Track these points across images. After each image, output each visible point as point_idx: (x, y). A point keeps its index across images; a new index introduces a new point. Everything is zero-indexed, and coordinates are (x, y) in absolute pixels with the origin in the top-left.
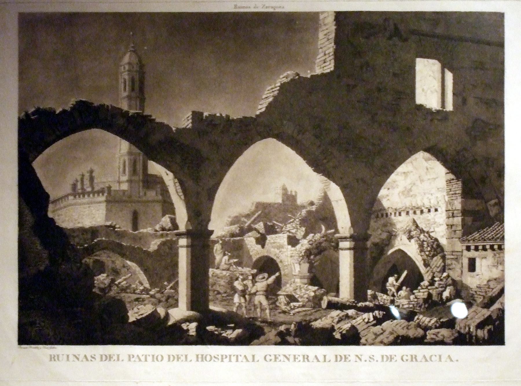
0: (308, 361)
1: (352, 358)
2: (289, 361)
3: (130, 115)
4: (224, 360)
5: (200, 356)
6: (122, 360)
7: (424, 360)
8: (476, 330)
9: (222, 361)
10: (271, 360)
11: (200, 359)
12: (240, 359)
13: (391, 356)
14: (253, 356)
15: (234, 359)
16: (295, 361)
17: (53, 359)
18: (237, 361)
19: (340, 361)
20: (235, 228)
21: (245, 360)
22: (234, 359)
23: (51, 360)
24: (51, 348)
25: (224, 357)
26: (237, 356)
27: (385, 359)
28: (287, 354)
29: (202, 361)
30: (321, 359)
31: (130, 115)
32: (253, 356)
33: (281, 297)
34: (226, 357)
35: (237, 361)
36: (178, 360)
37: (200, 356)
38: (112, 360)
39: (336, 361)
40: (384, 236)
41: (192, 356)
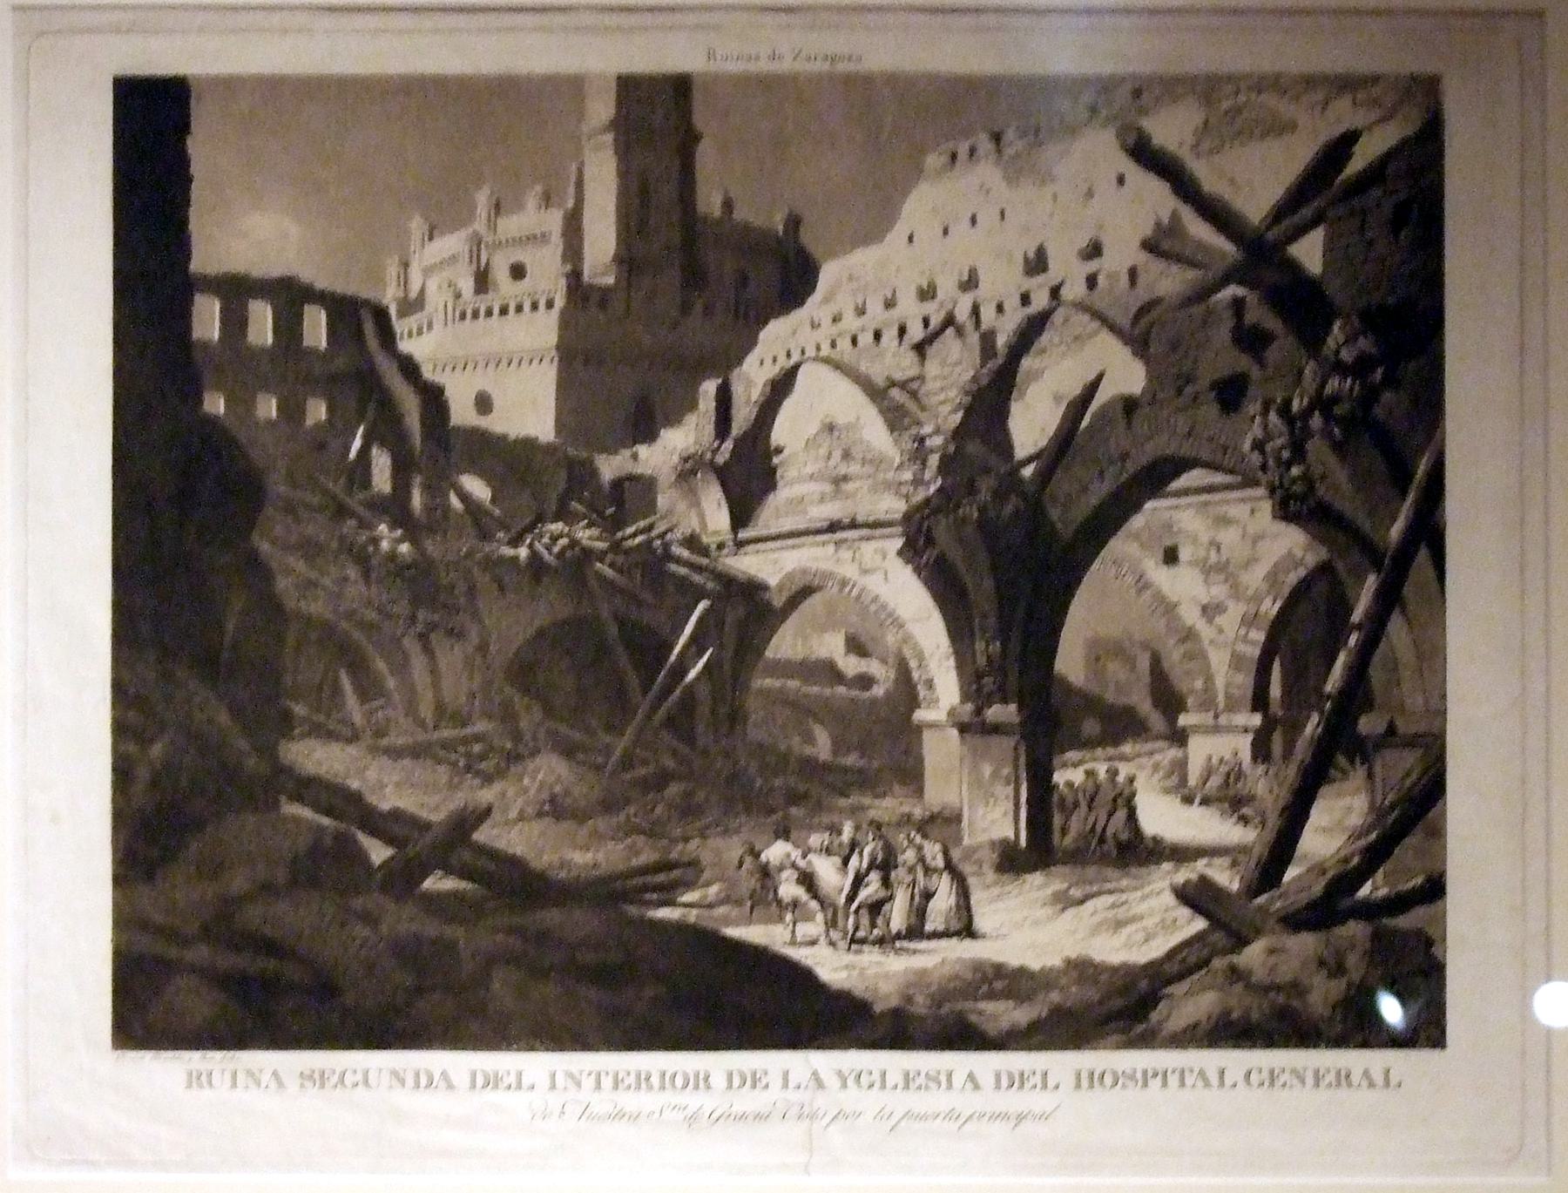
0: (1350, 1085)
1: (959, 1079)
2: (403, 1085)
3: (1374, 350)
4: (1151, 1082)
5: (1084, 1075)
6: (1054, 1085)
7: (1365, 1083)
8: (642, 849)
9: (1145, 1084)
10: (871, 1086)
11: (1085, 1083)
12: (1189, 1081)
13: (754, 1074)
14: (1222, 1073)
15: (1173, 1080)
16: (1317, 1084)
17: (643, 1085)
18: (1182, 1084)
19: (1112, 1087)
20: (538, 807)
21: (1200, 1083)
22: (1173, 1080)
23: (189, 1086)
24: (319, 1079)
25: (1150, 1074)
26: (1182, 1072)
27: (736, 1081)
28: (1299, 1067)
29: (1091, 1086)
30: (1378, 1078)
31: (1374, 350)
32: (1222, 1073)
33: (183, 982)
34: (1155, 1075)
35: (1182, 1084)
36: (754, 1086)
37: (1084, 1075)
38: (1027, 1085)
39: (730, 1086)
40: (1135, 133)
41: (461, 1079)
